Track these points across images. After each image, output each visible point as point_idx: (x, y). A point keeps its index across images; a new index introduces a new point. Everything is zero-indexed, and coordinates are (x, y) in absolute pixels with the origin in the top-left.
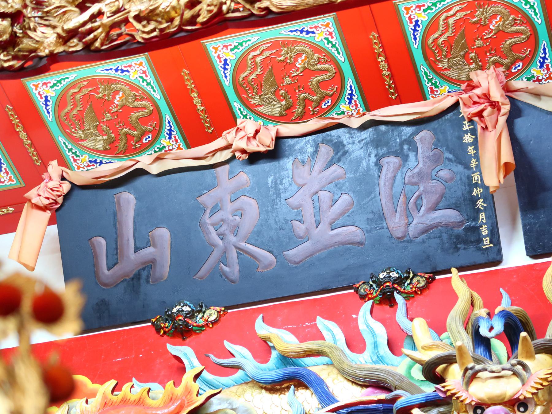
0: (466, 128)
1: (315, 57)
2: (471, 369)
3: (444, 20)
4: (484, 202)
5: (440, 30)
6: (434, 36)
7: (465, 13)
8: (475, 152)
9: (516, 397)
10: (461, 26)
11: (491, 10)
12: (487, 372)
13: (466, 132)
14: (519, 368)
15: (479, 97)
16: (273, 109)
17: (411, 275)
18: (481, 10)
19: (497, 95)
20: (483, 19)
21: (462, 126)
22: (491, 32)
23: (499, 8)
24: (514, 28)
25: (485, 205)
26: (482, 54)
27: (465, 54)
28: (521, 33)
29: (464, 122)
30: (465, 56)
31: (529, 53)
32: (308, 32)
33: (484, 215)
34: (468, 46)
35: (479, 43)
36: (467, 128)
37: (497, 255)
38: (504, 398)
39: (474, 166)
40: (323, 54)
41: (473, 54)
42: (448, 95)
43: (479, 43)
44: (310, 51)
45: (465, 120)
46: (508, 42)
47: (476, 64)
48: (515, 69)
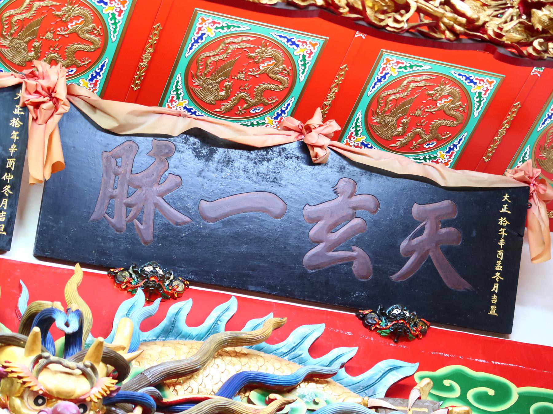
0: (17, 112)
1: (281, 67)
2: (46, 358)
3: (227, 44)
4: (11, 189)
5: (22, 9)
6: (208, 54)
7: (249, 45)
8: (18, 138)
9: (82, 398)
10: (43, 14)
11: (77, 10)
12: (61, 366)
13: (16, 116)
14: (89, 370)
15: (43, 89)
16: (207, 95)
17: (172, 277)
18: (70, 7)
19: (61, 93)
20: (67, 16)
21: (14, 108)
22: (257, 71)
23: (87, 12)
24: (88, 36)
25: (11, 193)
26: (47, 45)
27: (31, 40)
28: (92, 43)
29: (17, 106)
30: (29, 43)
31: (88, 64)
32: (294, 43)
33: (6, 202)
34: (37, 35)
35: (49, 35)
36: (18, 113)
37: (7, 244)
38: (72, 395)
39: (12, 152)
40: (100, 27)
41: (38, 44)
42: (12, 75)
43: (49, 35)
44: (90, 17)
45: (18, 104)
46: (75, 46)
47: (35, 54)
48: (253, 111)
